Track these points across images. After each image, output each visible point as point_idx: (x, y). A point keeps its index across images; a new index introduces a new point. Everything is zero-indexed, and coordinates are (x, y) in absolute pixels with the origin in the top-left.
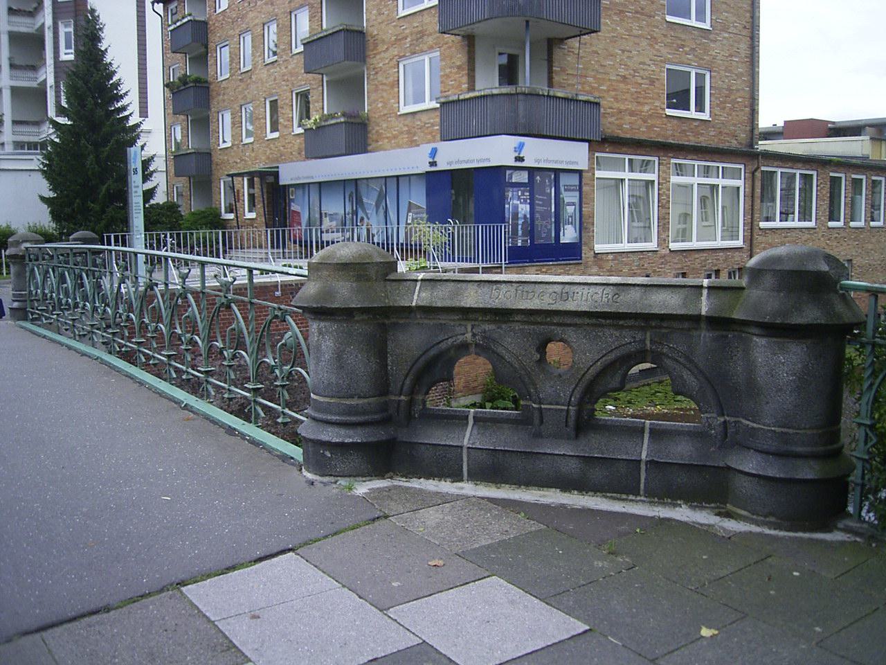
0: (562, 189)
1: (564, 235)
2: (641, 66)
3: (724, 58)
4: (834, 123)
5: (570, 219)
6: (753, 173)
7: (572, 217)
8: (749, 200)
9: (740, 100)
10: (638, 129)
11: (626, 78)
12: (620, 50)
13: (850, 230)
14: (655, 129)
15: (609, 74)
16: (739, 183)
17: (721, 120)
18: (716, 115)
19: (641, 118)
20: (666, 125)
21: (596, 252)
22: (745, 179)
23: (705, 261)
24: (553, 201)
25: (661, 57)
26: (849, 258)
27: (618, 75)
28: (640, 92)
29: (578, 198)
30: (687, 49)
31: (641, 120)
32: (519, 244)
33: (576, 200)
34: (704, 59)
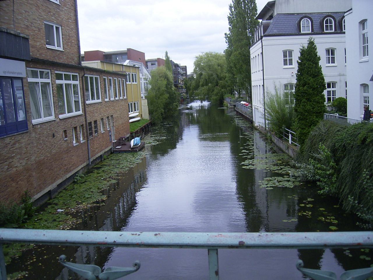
0: (15, 89)
1: (19, 116)
2: (34, 21)
3: (66, 20)
4: (104, 52)
5: (21, 106)
6: (82, 77)
7: (21, 105)
8: (82, 90)
9: (73, 41)
10: (36, 55)
11: (28, 27)
12: (24, 11)
13: (111, 102)
14: (43, 55)
15: (20, 24)
16: (77, 83)
17: (68, 51)
18: (65, 49)
19: (37, 49)
20: (47, 53)
21: (34, 124)
22: (80, 80)
24: (12, 95)
25: (42, 16)
26: (112, 114)
27: (25, 25)
28: (35, 35)
29: (22, 94)
30: (52, 14)
31: (36, 50)
33: (22, 95)
34: (58, 20)
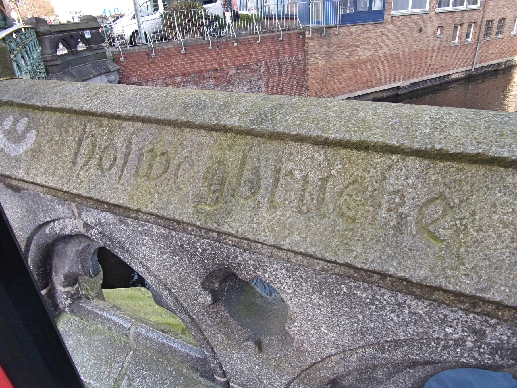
23: (455, 18)
32: (348, 12)
